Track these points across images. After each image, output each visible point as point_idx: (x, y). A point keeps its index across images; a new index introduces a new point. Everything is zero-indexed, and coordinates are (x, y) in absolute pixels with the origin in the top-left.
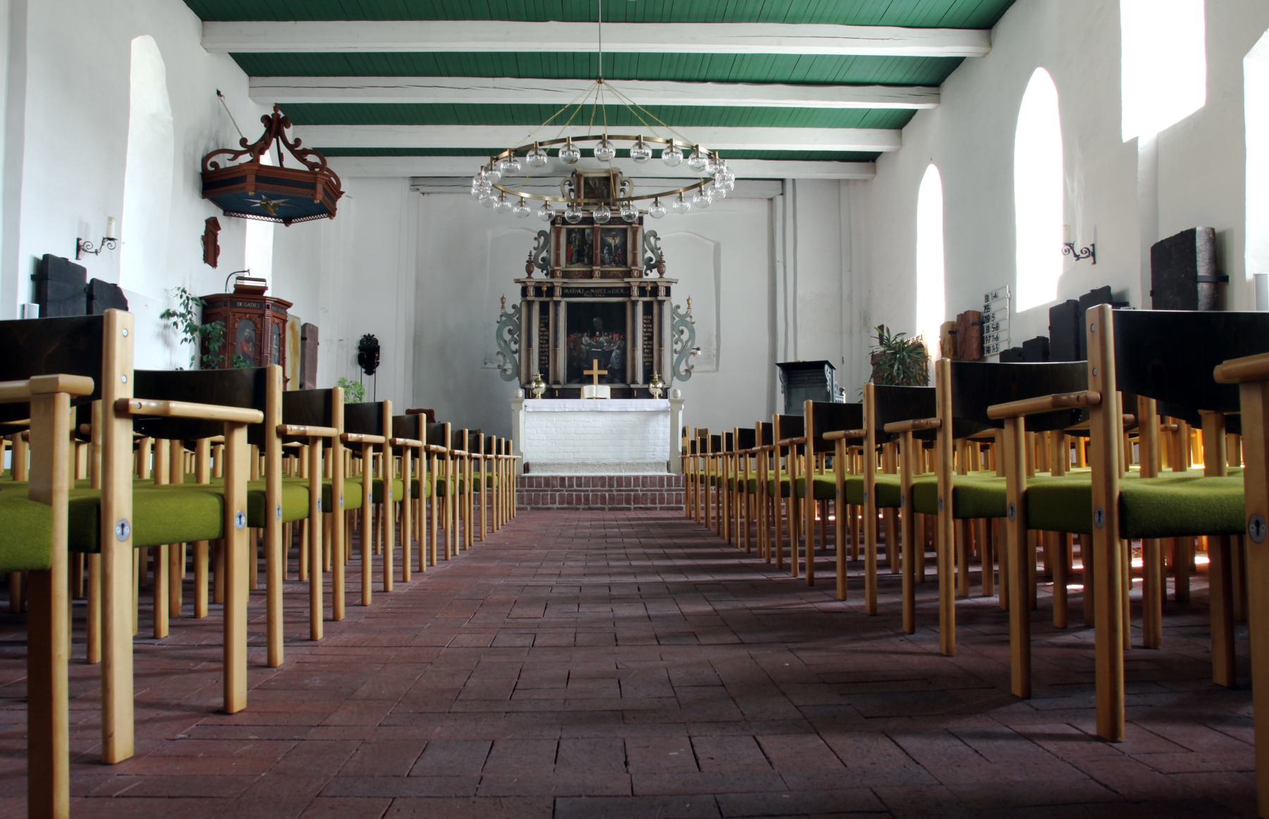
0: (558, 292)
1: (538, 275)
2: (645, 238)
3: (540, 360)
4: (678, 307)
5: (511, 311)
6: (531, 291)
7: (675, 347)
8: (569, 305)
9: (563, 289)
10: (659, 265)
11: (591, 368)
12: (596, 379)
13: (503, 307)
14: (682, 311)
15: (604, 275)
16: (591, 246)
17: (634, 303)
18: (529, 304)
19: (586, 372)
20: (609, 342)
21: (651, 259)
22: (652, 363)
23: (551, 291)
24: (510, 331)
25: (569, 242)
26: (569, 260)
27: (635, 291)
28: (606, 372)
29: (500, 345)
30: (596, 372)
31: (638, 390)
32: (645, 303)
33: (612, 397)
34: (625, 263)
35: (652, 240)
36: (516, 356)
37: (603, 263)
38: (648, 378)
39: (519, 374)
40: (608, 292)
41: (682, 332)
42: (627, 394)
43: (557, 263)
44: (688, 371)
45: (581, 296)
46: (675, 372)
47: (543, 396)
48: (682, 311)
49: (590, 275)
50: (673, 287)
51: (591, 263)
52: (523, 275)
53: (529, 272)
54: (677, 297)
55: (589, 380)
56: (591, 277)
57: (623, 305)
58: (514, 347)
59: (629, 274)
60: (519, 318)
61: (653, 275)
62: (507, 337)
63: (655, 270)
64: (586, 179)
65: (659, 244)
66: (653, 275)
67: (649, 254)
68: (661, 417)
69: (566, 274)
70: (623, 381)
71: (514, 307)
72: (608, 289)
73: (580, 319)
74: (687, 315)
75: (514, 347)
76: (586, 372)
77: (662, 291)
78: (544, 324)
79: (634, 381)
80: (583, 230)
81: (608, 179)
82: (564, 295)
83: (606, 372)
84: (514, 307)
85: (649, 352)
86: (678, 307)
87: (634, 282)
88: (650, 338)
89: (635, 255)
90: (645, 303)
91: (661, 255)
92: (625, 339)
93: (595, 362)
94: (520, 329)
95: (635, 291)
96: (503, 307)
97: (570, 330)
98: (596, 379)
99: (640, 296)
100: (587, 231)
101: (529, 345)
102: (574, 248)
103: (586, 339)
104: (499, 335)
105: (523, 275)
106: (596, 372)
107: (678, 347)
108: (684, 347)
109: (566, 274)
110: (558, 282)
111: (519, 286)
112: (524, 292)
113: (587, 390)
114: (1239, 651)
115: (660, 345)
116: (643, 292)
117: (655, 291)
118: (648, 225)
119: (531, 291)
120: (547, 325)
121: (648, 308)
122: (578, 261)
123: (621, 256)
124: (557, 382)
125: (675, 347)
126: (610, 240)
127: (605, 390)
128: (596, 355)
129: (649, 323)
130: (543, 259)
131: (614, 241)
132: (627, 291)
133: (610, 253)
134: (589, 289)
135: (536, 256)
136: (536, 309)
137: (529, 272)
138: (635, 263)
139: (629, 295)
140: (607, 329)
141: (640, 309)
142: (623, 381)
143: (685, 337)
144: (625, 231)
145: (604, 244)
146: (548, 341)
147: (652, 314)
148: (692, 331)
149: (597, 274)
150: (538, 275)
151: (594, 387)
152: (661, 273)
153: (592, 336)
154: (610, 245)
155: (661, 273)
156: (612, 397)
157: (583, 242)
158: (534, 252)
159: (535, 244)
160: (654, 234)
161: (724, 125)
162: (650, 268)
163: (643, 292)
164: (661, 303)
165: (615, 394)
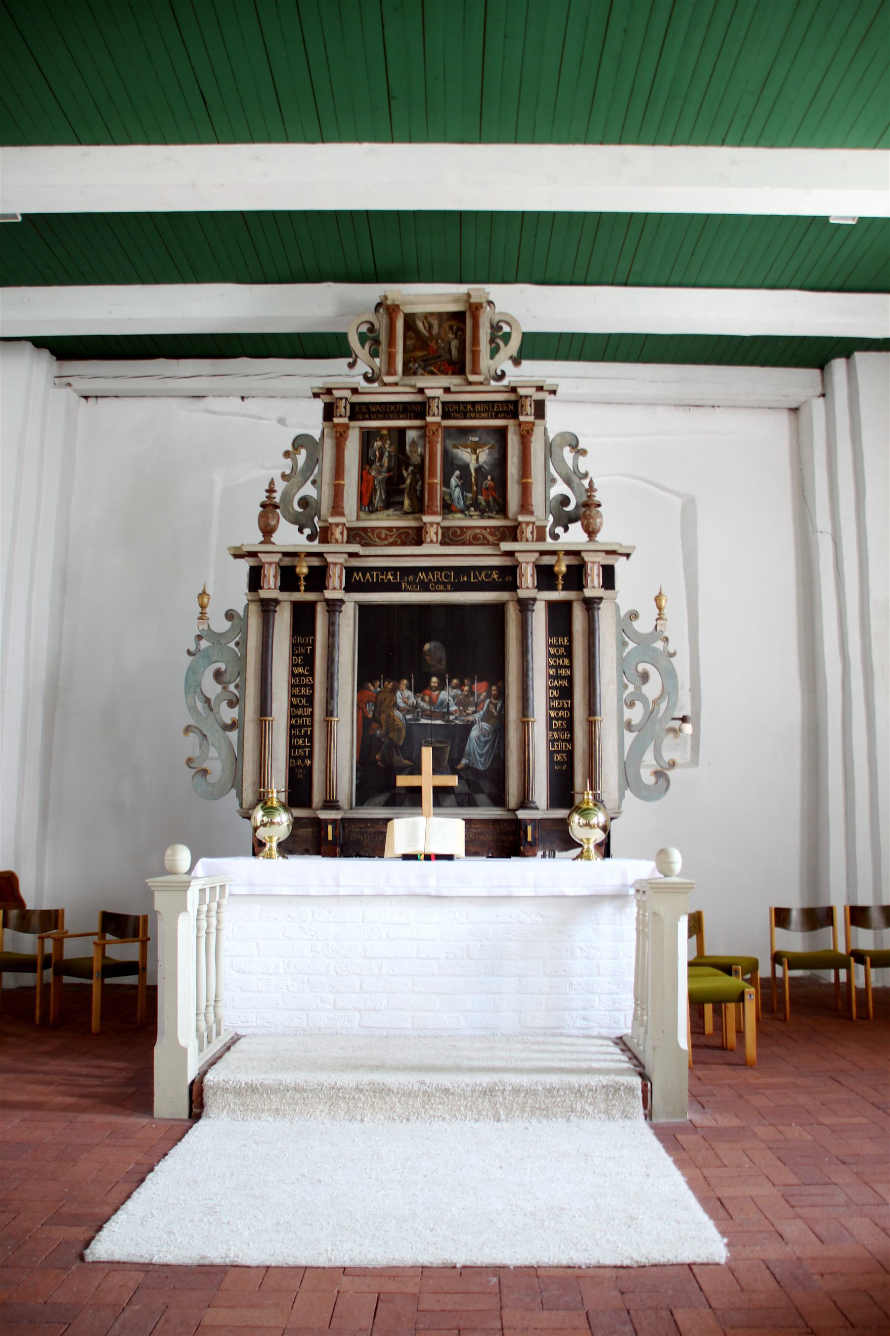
0: (336, 578)
1: (289, 536)
2: (549, 449)
3: (292, 747)
4: (634, 615)
5: (221, 625)
6: (271, 578)
7: (628, 714)
8: (364, 610)
9: (350, 571)
10: (585, 512)
11: (416, 770)
12: (427, 796)
13: (202, 616)
14: (644, 625)
15: (450, 537)
16: (420, 469)
17: (525, 606)
18: (268, 608)
19: (403, 781)
20: (463, 703)
21: (565, 501)
22: (570, 754)
23: (318, 578)
24: (218, 675)
25: (366, 461)
26: (366, 504)
27: (528, 577)
28: (452, 781)
29: (193, 709)
30: (427, 780)
31: (538, 823)
32: (552, 606)
33: (472, 850)
34: (502, 510)
35: (568, 455)
36: (233, 735)
37: (448, 508)
38: (563, 792)
39: (237, 783)
40: (460, 578)
41: (645, 677)
42: (504, 840)
43: (337, 508)
44: (659, 774)
45: (396, 588)
46: (628, 779)
47: (287, 848)
48: (644, 625)
49: (417, 537)
50: (620, 566)
51: (419, 508)
52: (253, 538)
53: (268, 531)
54: (631, 591)
55: (411, 798)
56: (419, 542)
57: (499, 609)
58: (228, 714)
59: (513, 533)
60: (242, 644)
61: (574, 536)
62: (212, 688)
63: (576, 528)
64: (410, 320)
65: (584, 464)
66: (574, 536)
67: (560, 488)
68: (607, 910)
69: (356, 535)
70: (499, 800)
71: (230, 615)
72: (460, 570)
73: (391, 644)
74: (656, 633)
75: (228, 714)
76: (403, 781)
77: (594, 577)
78: (303, 657)
79: (525, 802)
80: (402, 431)
81: (458, 317)
82: (350, 587)
83: (452, 781)
84: (230, 615)
85: (562, 727)
86: (634, 615)
87: (526, 554)
88: (567, 693)
89: (525, 490)
90: (552, 606)
91: (591, 488)
92: (502, 695)
93: (427, 754)
94: (242, 672)
95: (528, 577)
96: (202, 616)
97: (369, 669)
98: (427, 796)
99: (540, 587)
100: (411, 435)
101: (264, 708)
102: (378, 475)
103: (405, 696)
104: (192, 685)
105: (253, 538)
106: (427, 780)
107: (636, 714)
108: (650, 714)
109: (356, 535)
110: (338, 553)
111: (244, 566)
112: (255, 579)
113: (406, 830)
114: (330, 708)
115: (592, 709)
116: (546, 577)
117: (576, 577)
118: (557, 420)
119: (271, 578)
120: (309, 661)
121: (560, 616)
122: (388, 504)
123: (492, 492)
124: (330, 804)
125: (628, 714)
126: (465, 455)
127: (447, 830)
128: (432, 735)
129: (562, 654)
130: (304, 502)
131: (475, 458)
132: (507, 577)
133: (465, 486)
134: (415, 570)
135: (287, 496)
136: (283, 620)
137: (268, 531)
138: (525, 507)
139: (513, 586)
140: (459, 669)
141: (539, 619)
142: (499, 800)
143: (652, 689)
144: (502, 433)
145: (450, 464)
146: (310, 699)
147: (568, 632)
148: (669, 676)
149: (432, 533)
150: (289, 536)
151: (420, 821)
152: (591, 533)
153: (420, 687)
154: (465, 468)
155: (591, 533)
156: (472, 850)
157: (401, 458)
158: (280, 486)
159: (286, 465)
160: (574, 445)
161: (757, 143)
162: (565, 521)
163: (546, 577)
164: (591, 605)
165: (476, 846)
